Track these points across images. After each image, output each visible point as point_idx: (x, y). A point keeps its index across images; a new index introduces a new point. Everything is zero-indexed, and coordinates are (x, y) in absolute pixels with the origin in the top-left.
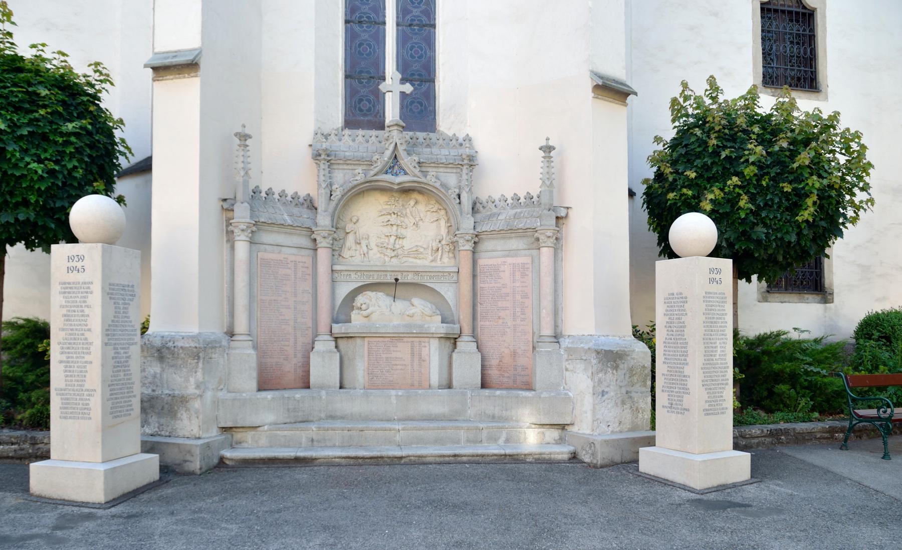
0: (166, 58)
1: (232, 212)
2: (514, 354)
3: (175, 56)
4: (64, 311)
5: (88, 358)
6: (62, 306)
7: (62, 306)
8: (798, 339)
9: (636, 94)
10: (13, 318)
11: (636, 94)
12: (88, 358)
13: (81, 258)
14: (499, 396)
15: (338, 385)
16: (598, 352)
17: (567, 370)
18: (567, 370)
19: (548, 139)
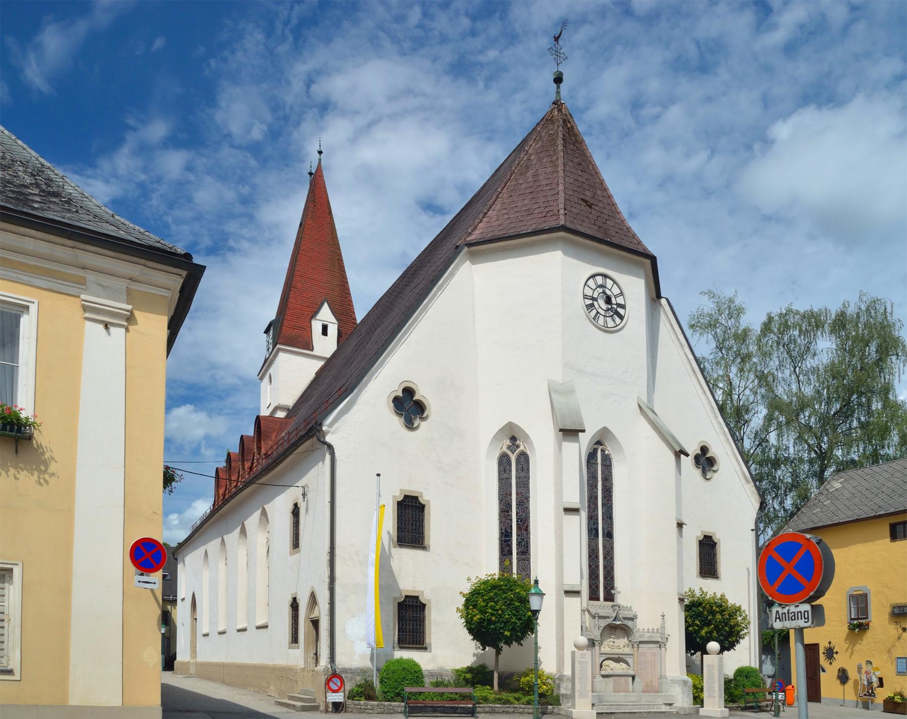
0: (571, 588)
1: (855, 706)
2: (651, 682)
3: (573, 587)
4: (580, 669)
5: (587, 682)
6: (579, 668)
7: (579, 668)
8: (748, 665)
9: (686, 525)
10: (292, 713)
11: (686, 525)
12: (587, 682)
13: (585, 655)
14: (652, 695)
15: (636, 679)
16: (683, 681)
17: (671, 686)
18: (671, 686)
19: (663, 613)
